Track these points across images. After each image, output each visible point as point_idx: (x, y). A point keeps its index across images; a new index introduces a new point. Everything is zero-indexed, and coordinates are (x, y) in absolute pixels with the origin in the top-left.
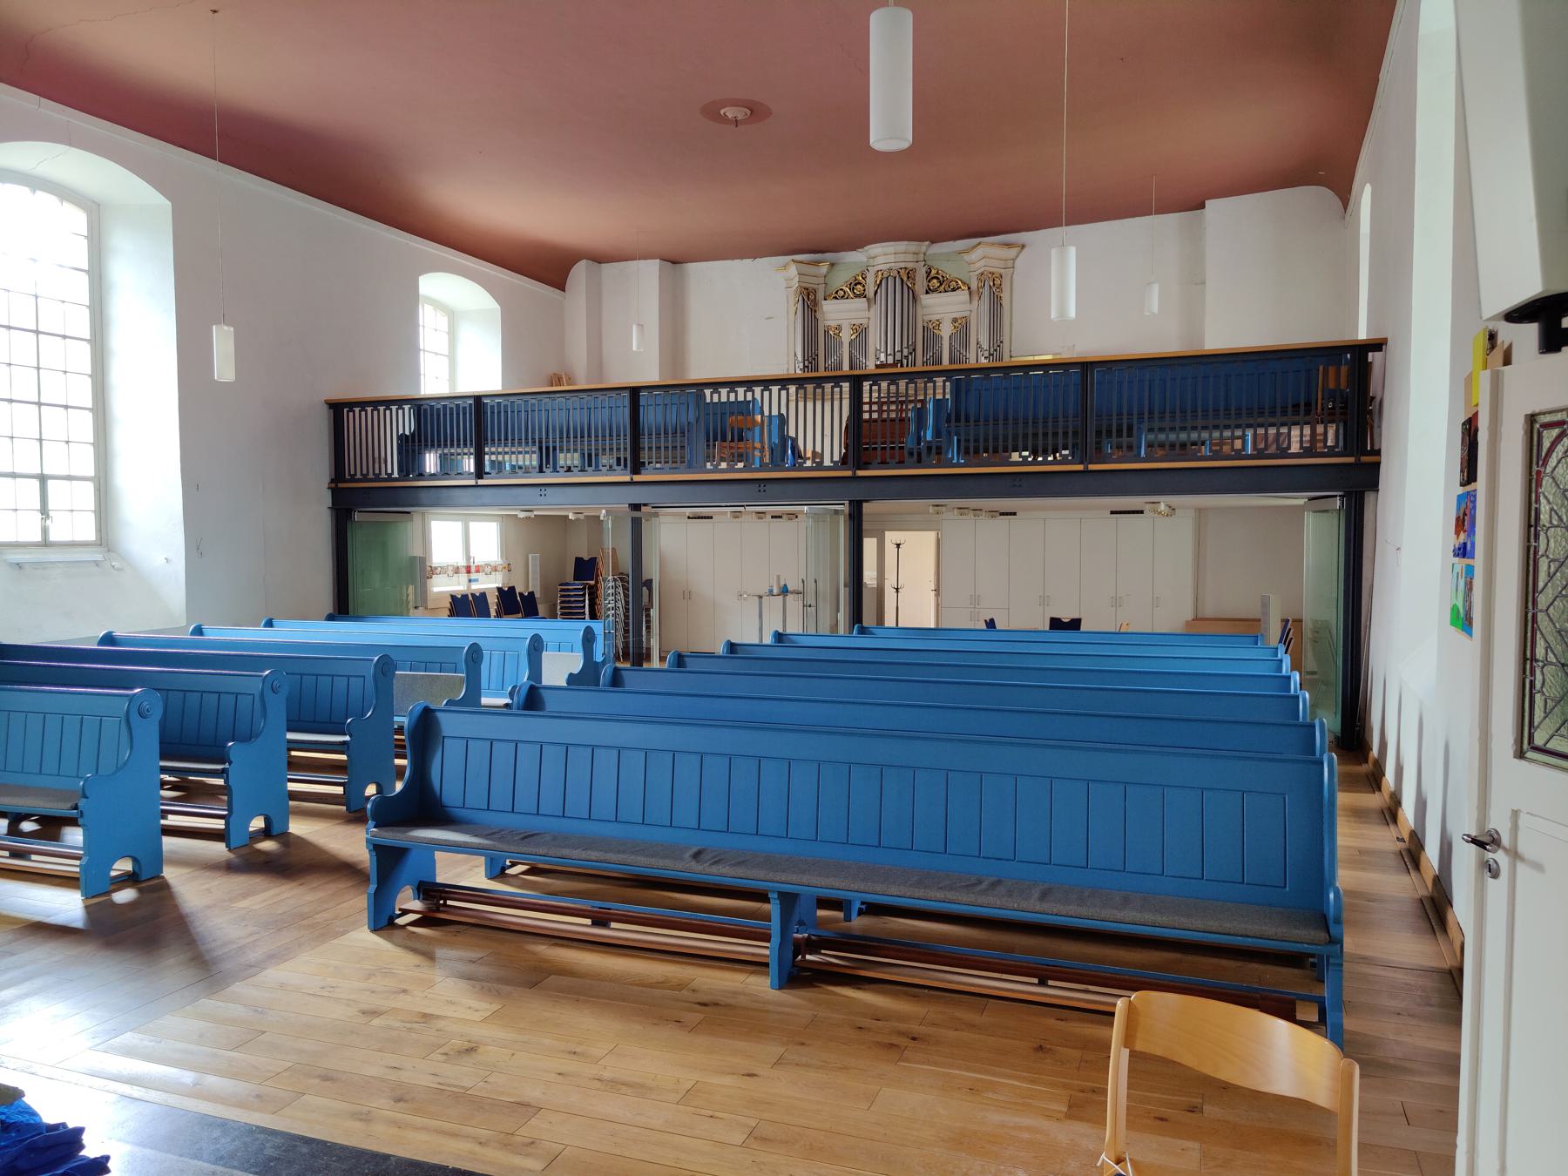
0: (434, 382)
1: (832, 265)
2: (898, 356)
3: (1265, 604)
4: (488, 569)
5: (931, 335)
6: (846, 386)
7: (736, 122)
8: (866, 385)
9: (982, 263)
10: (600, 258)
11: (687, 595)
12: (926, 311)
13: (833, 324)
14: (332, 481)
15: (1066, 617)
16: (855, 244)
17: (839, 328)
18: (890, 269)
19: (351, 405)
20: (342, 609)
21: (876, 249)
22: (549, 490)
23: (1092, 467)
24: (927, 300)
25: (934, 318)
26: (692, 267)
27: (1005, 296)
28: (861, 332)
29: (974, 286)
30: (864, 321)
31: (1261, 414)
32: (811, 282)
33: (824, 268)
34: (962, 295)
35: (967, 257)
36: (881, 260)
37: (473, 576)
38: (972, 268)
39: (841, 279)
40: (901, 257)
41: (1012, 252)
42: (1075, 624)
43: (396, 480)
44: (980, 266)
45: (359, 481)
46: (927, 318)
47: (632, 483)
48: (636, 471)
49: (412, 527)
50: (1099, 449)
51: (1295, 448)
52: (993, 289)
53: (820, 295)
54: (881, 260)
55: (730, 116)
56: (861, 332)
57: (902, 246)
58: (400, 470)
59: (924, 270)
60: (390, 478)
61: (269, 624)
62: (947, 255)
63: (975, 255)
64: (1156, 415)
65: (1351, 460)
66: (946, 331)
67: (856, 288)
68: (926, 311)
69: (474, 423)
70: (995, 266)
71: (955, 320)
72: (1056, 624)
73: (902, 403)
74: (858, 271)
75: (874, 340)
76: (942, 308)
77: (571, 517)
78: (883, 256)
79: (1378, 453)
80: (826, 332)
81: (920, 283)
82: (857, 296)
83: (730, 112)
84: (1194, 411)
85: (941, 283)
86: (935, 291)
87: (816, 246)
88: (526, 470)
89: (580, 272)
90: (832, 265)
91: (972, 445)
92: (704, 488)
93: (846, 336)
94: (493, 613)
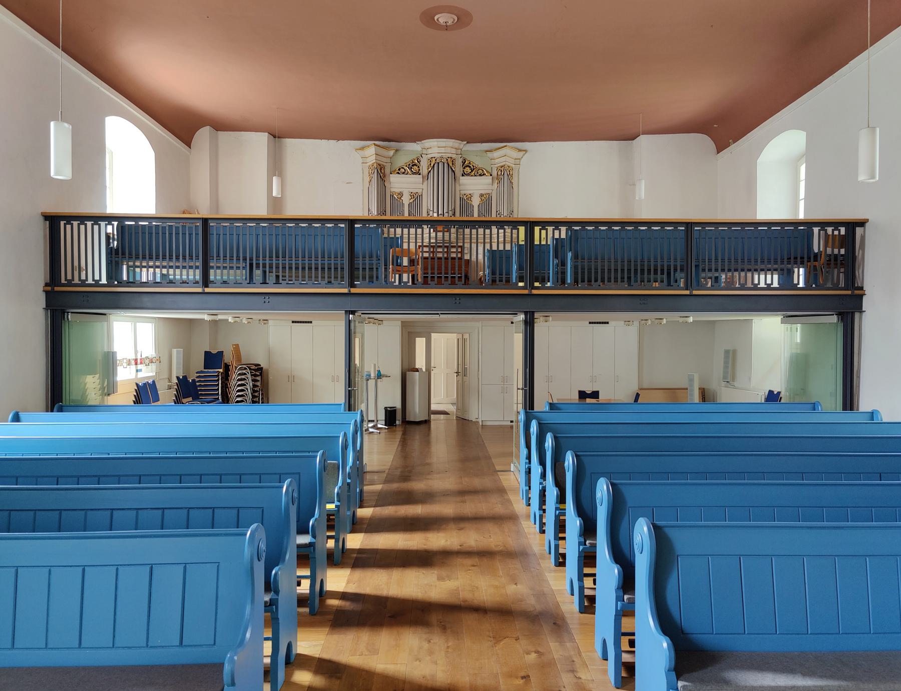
0: (115, 205)
1: (397, 150)
3: (691, 380)
4: (147, 361)
5: (465, 202)
6: (522, 229)
7: (447, 28)
8: (537, 229)
9: (503, 159)
10: (220, 125)
11: (291, 378)
12: (462, 187)
14: (46, 285)
15: (589, 390)
16: (416, 138)
17: (401, 194)
19: (69, 219)
20: (57, 397)
21: (428, 143)
22: (272, 298)
23: (695, 292)
24: (464, 180)
25: (468, 192)
26: (289, 142)
27: (515, 181)
28: (417, 198)
29: (495, 173)
30: (420, 191)
31: (769, 262)
33: (392, 153)
34: (487, 180)
37: (140, 367)
39: (402, 160)
40: (449, 150)
42: (595, 395)
43: (103, 286)
44: (500, 162)
45: (64, 285)
46: (463, 192)
47: (349, 294)
48: (352, 285)
49: (97, 326)
50: (698, 281)
51: (762, 285)
52: (505, 175)
53: (387, 171)
54: (436, 150)
55: (442, 21)
56: (417, 198)
57: (450, 143)
58: (109, 277)
59: (461, 160)
60: (97, 284)
61: (17, 418)
62: (475, 152)
63: (496, 154)
64: (740, 261)
65: (849, 292)
67: (413, 167)
68: (462, 187)
69: (134, 241)
70: (510, 162)
71: (482, 195)
72: (583, 395)
73: (433, 247)
76: (474, 187)
77: (231, 320)
78: (436, 148)
79: (862, 288)
80: (392, 196)
81: (458, 169)
82: (414, 173)
83: (442, 18)
84: (743, 259)
85: (471, 170)
86: (468, 175)
87: (388, 136)
88: (237, 284)
89: (204, 135)
90: (397, 150)
91: (504, 276)
92: (368, 299)
93: (406, 200)
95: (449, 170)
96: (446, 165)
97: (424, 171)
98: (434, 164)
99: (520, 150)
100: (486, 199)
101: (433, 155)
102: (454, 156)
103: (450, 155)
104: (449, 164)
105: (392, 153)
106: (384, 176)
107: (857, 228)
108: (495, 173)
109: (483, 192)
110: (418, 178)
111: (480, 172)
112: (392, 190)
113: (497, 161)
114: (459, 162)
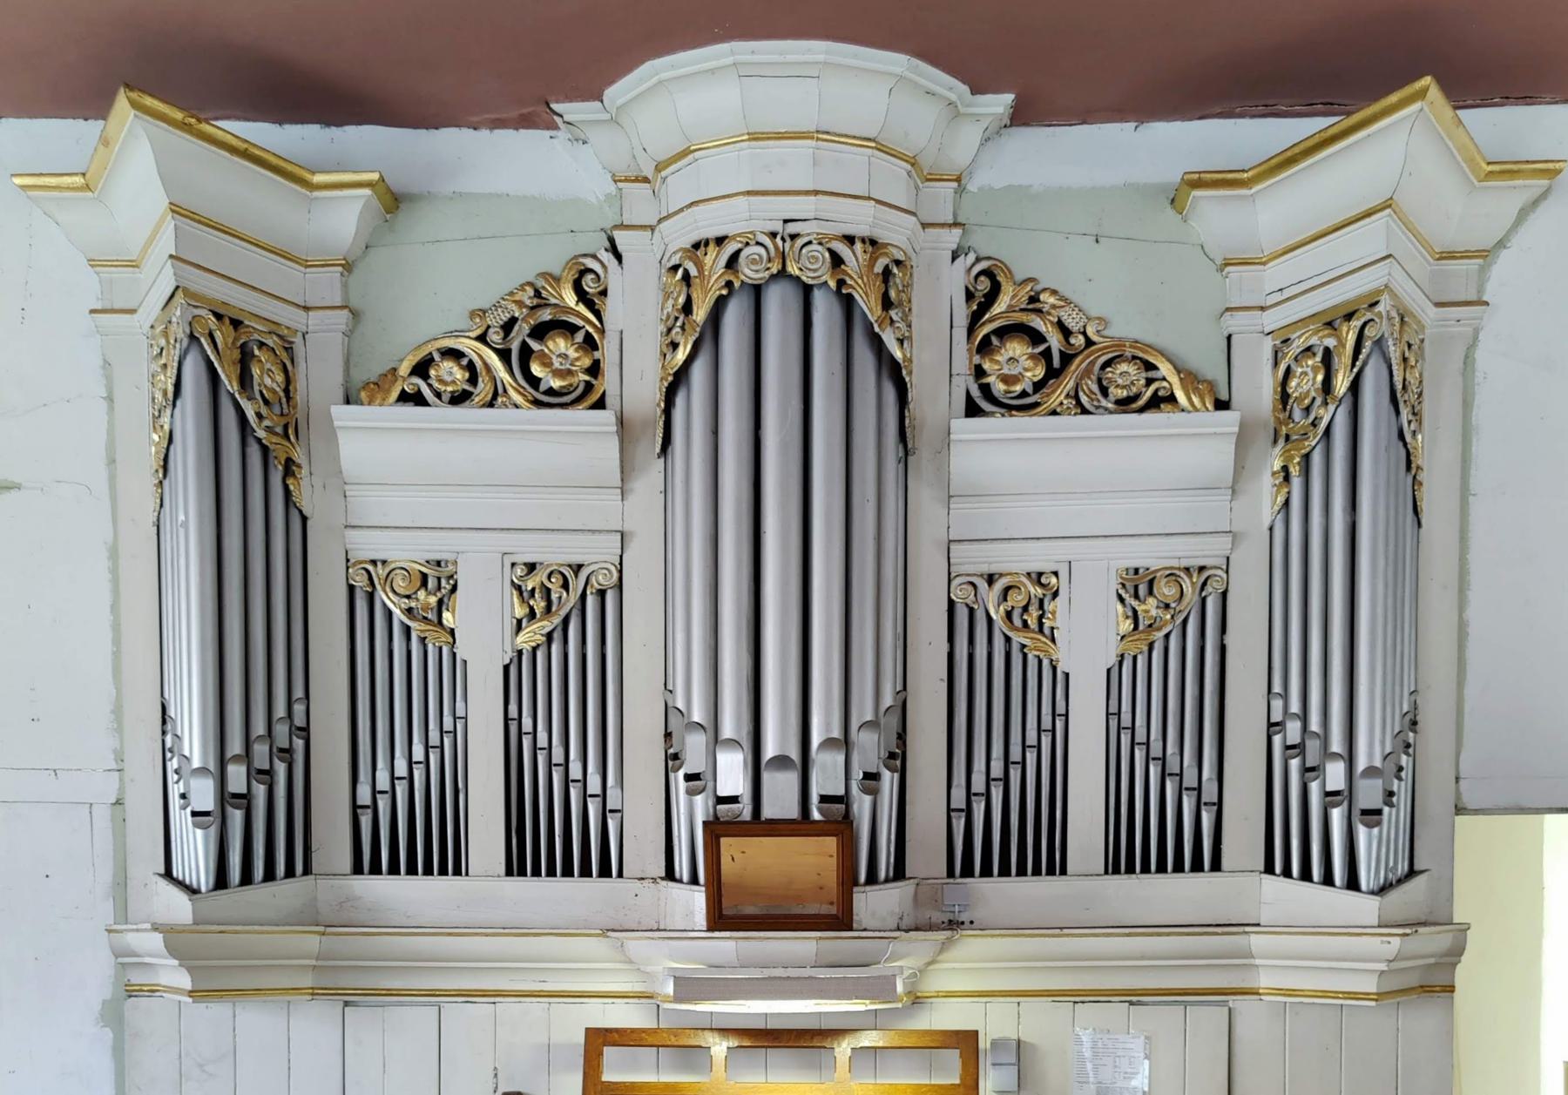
1: (393, 200)
2: (827, 776)
5: (998, 636)
12: (965, 517)
13: (407, 551)
17: (439, 581)
18: (786, 237)
24: (989, 451)
25: (1016, 560)
27: (1436, 450)
28: (571, 610)
30: (597, 554)
32: (262, 289)
34: (1191, 443)
35: (1215, 217)
36: (724, 169)
38: (1244, 285)
39: (448, 289)
41: (1508, 198)
46: (973, 559)
52: (1354, 401)
53: (319, 374)
54: (724, 169)
56: (571, 610)
59: (954, 279)
66: (1087, 637)
67: (540, 345)
68: (965, 517)
71: (1138, 584)
74: (554, 257)
75: (661, 659)
76: (1072, 507)
80: (360, 599)
85: (1042, 357)
86: (1022, 406)
93: (484, 631)
94: (1170, 867)
95: (837, 345)
96: (825, 311)
97: (637, 374)
98: (723, 299)
99: (1508, 170)
100: (1176, 614)
101: (707, 223)
102: (897, 232)
103: (860, 219)
104: (855, 300)
105: (342, 218)
106: (290, 429)
107: (723, 840)
108: (1256, 386)
109: (1150, 555)
110: (584, 437)
111: (1126, 376)
112: (367, 545)
113: (1278, 274)
114: (939, 295)
